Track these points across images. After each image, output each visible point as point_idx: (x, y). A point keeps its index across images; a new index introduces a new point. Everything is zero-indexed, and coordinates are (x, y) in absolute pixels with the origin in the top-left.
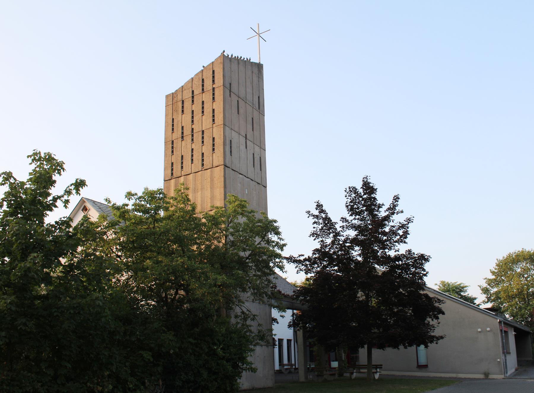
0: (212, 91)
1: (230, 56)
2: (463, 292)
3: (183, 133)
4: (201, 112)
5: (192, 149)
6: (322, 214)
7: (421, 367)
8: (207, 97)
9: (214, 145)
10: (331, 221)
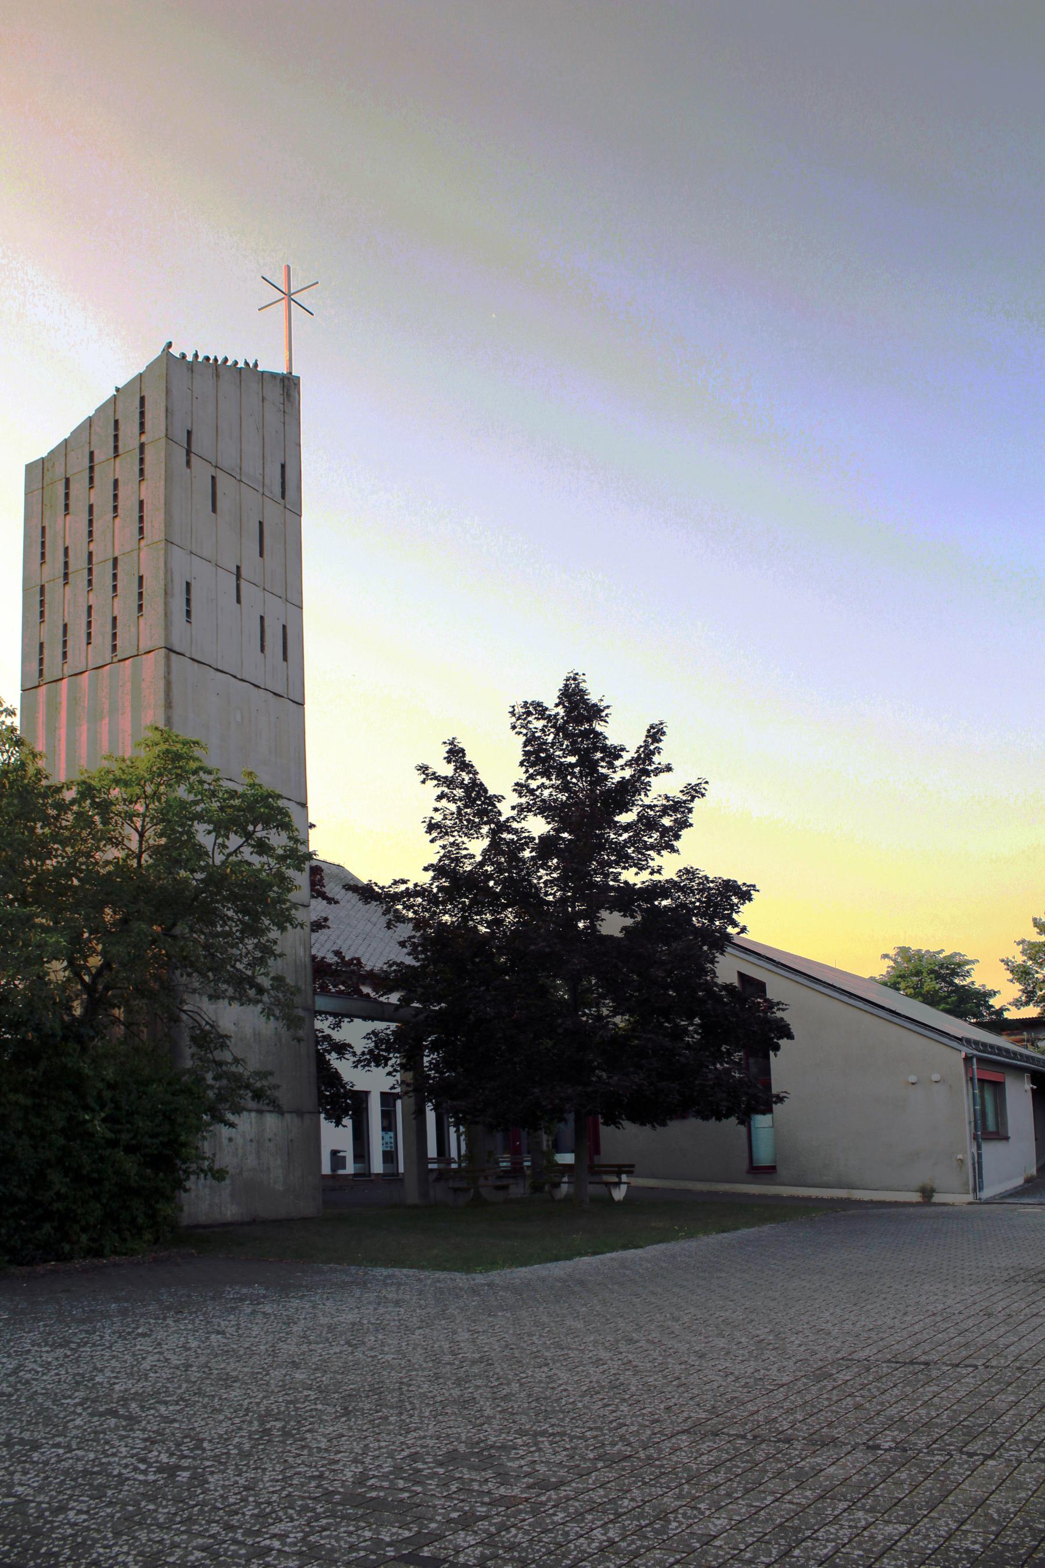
0: (137, 451)
1: (190, 358)
2: (958, 976)
3: (66, 564)
4: (111, 508)
5: (90, 608)
6: (464, 774)
7: (768, 1172)
8: (126, 468)
9: (141, 594)
10: (486, 791)
